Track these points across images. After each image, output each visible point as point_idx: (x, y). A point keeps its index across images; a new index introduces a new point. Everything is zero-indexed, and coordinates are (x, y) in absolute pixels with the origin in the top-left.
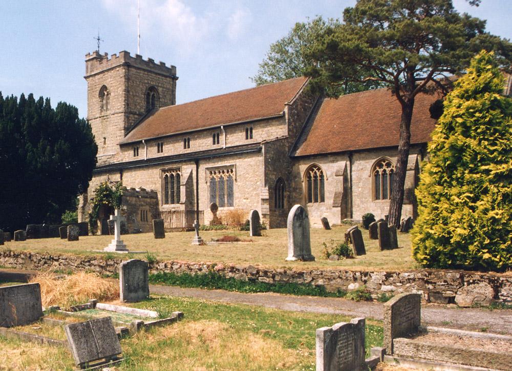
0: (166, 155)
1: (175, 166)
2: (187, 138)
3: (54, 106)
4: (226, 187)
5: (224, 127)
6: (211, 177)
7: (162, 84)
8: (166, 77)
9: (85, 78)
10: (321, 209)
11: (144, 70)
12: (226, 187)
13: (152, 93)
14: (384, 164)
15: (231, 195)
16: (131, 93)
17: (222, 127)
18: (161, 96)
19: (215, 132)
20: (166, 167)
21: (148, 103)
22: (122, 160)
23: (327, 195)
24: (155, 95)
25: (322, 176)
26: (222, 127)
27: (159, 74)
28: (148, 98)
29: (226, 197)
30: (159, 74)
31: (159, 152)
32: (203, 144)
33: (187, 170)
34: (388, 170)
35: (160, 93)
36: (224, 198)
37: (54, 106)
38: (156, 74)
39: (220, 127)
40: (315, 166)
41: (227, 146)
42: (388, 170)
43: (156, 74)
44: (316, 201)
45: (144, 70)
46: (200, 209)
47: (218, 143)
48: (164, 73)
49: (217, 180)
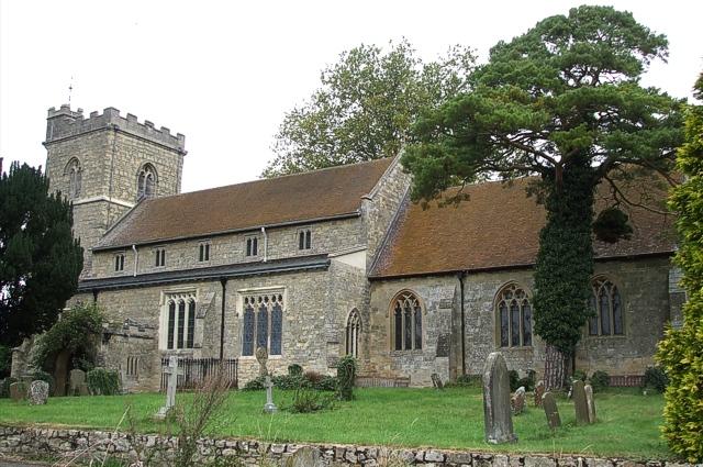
0: (169, 269)
1: (187, 287)
2: (161, 249)
3: (86, 116)
4: (270, 324)
5: (266, 229)
6: (246, 306)
7: (163, 160)
8: (170, 149)
9: (43, 144)
10: (417, 359)
11: (139, 138)
12: (270, 324)
13: (149, 173)
14: (514, 291)
15: (277, 337)
16: (117, 172)
17: (263, 229)
18: (160, 179)
19: (249, 233)
20: (173, 289)
21: (141, 188)
22: (94, 275)
23: (425, 337)
24: (152, 177)
25: (417, 308)
26: (263, 229)
27: (160, 145)
28: (141, 181)
29: (255, 339)
30: (160, 145)
31: (249, 254)
32: (229, 253)
33: (205, 294)
34: (519, 302)
35: (160, 174)
36: (266, 340)
37: (86, 116)
38: (155, 144)
39: (260, 229)
40: (407, 293)
41: (269, 258)
42: (519, 302)
43: (155, 144)
44: (408, 347)
45: (139, 138)
46: (226, 357)
47: (255, 254)
48: (169, 146)
49: (256, 311)
